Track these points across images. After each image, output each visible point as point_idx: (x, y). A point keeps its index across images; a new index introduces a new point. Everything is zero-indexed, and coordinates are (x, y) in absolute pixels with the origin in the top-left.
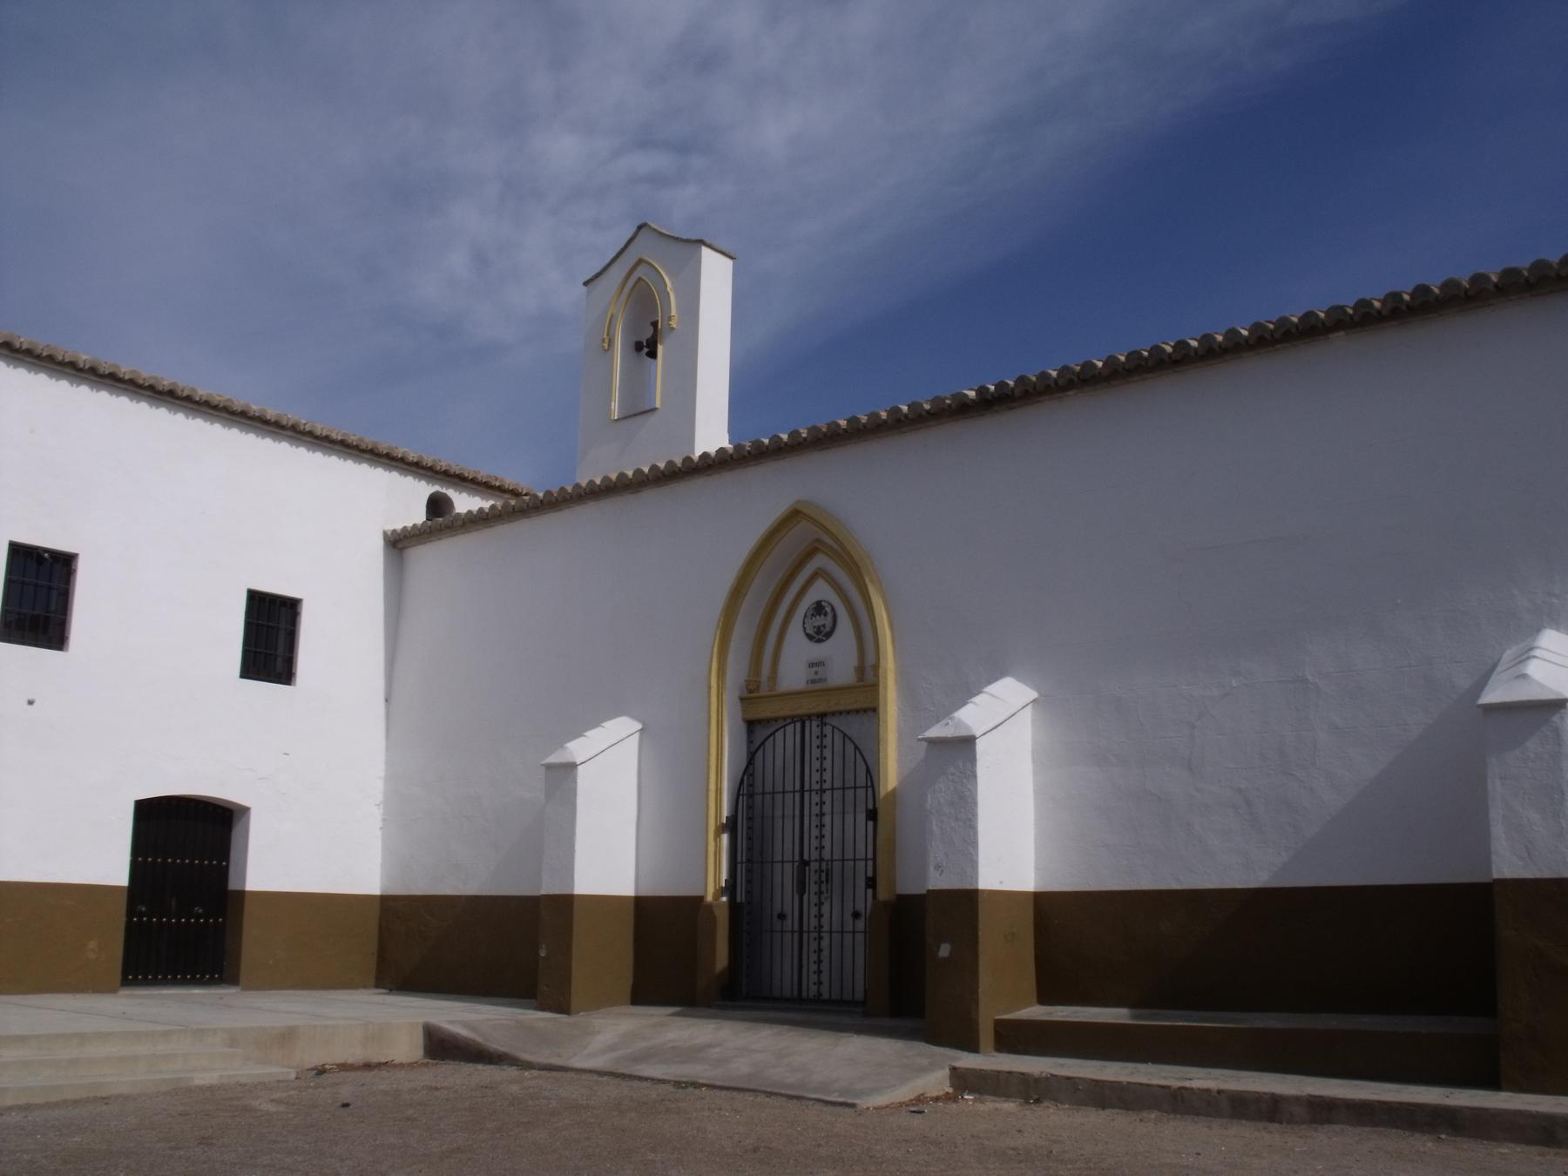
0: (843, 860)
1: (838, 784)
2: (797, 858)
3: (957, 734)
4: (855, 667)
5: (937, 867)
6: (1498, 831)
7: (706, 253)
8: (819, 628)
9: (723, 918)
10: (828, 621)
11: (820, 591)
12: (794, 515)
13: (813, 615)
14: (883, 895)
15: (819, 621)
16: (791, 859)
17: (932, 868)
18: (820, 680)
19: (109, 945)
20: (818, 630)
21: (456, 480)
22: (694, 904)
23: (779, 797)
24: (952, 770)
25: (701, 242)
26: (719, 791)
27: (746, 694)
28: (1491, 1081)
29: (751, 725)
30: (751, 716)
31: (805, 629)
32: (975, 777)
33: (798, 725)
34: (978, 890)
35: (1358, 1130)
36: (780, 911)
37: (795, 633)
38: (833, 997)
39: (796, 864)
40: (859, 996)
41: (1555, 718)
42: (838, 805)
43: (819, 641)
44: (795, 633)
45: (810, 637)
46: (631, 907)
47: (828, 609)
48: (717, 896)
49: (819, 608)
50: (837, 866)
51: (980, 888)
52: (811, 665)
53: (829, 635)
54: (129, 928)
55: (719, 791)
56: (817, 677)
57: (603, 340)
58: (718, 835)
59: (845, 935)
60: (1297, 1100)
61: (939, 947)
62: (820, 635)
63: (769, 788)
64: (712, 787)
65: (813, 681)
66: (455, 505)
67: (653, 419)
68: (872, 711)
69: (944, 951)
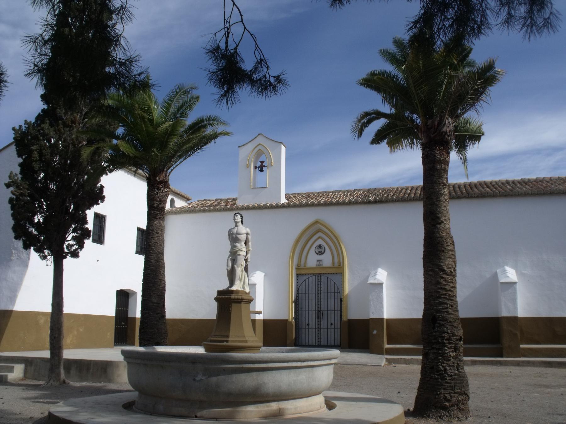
0: (334, 311)
1: (326, 291)
2: (317, 310)
3: (378, 282)
4: (12, 227)
5: (372, 313)
6: (503, 307)
7: (282, 145)
8: (320, 251)
9: (294, 324)
10: (323, 250)
11: (320, 242)
12: (316, 222)
13: (318, 248)
14: (345, 319)
15: (320, 250)
16: (337, 309)
17: (371, 313)
18: (321, 265)
19: (111, 335)
20: (320, 252)
21: (177, 195)
22: (286, 321)
23: (307, 295)
24: (376, 290)
25: (282, 143)
26: (292, 292)
27: (297, 267)
28: (502, 356)
29: (298, 275)
30: (298, 273)
31: (315, 251)
32: (383, 292)
33: (317, 276)
34: (136, 318)
35: (482, 366)
36: (308, 323)
37: (312, 251)
38: (325, 345)
39: (316, 312)
40: (336, 344)
41: (515, 285)
42: (326, 297)
43: (320, 255)
44: (312, 251)
45: (317, 254)
46: (262, 321)
47: (323, 247)
48: (292, 320)
49: (320, 246)
50: (326, 312)
51: (137, 317)
52: (318, 261)
53: (323, 253)
54: (116, 329)
55: (292, 292)
56: (320, 264)
57: (247, 165)
58: (292, 304)
59: (313, 329)
60: (469, 361)
61: (373, 331)
62: (320, 253)
63: (304, 292)
64: (291, 291)
65: (319, 265)
66: (175, 202)
67: (266, 189)
68: (342, 274)
69: (375, 332)
